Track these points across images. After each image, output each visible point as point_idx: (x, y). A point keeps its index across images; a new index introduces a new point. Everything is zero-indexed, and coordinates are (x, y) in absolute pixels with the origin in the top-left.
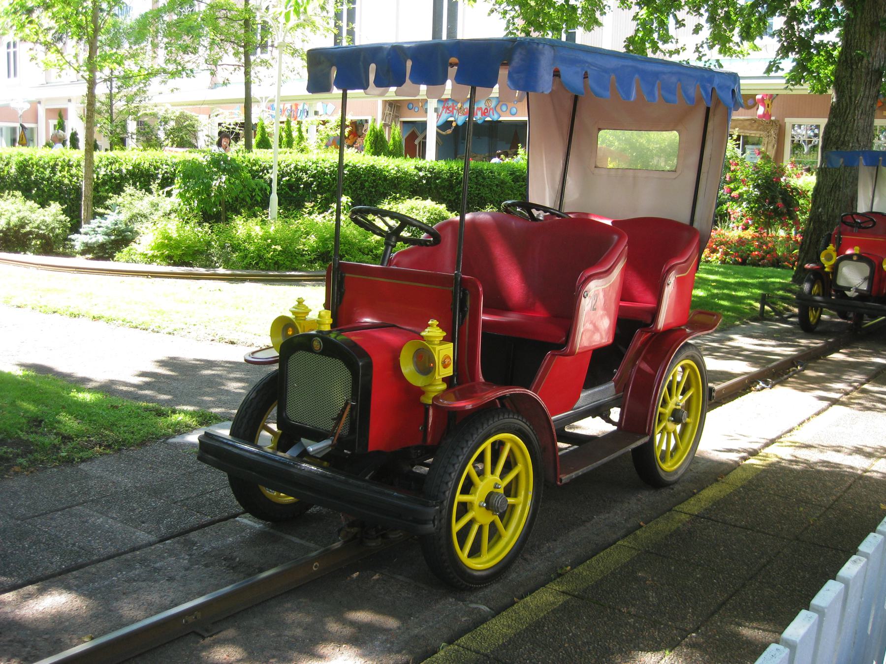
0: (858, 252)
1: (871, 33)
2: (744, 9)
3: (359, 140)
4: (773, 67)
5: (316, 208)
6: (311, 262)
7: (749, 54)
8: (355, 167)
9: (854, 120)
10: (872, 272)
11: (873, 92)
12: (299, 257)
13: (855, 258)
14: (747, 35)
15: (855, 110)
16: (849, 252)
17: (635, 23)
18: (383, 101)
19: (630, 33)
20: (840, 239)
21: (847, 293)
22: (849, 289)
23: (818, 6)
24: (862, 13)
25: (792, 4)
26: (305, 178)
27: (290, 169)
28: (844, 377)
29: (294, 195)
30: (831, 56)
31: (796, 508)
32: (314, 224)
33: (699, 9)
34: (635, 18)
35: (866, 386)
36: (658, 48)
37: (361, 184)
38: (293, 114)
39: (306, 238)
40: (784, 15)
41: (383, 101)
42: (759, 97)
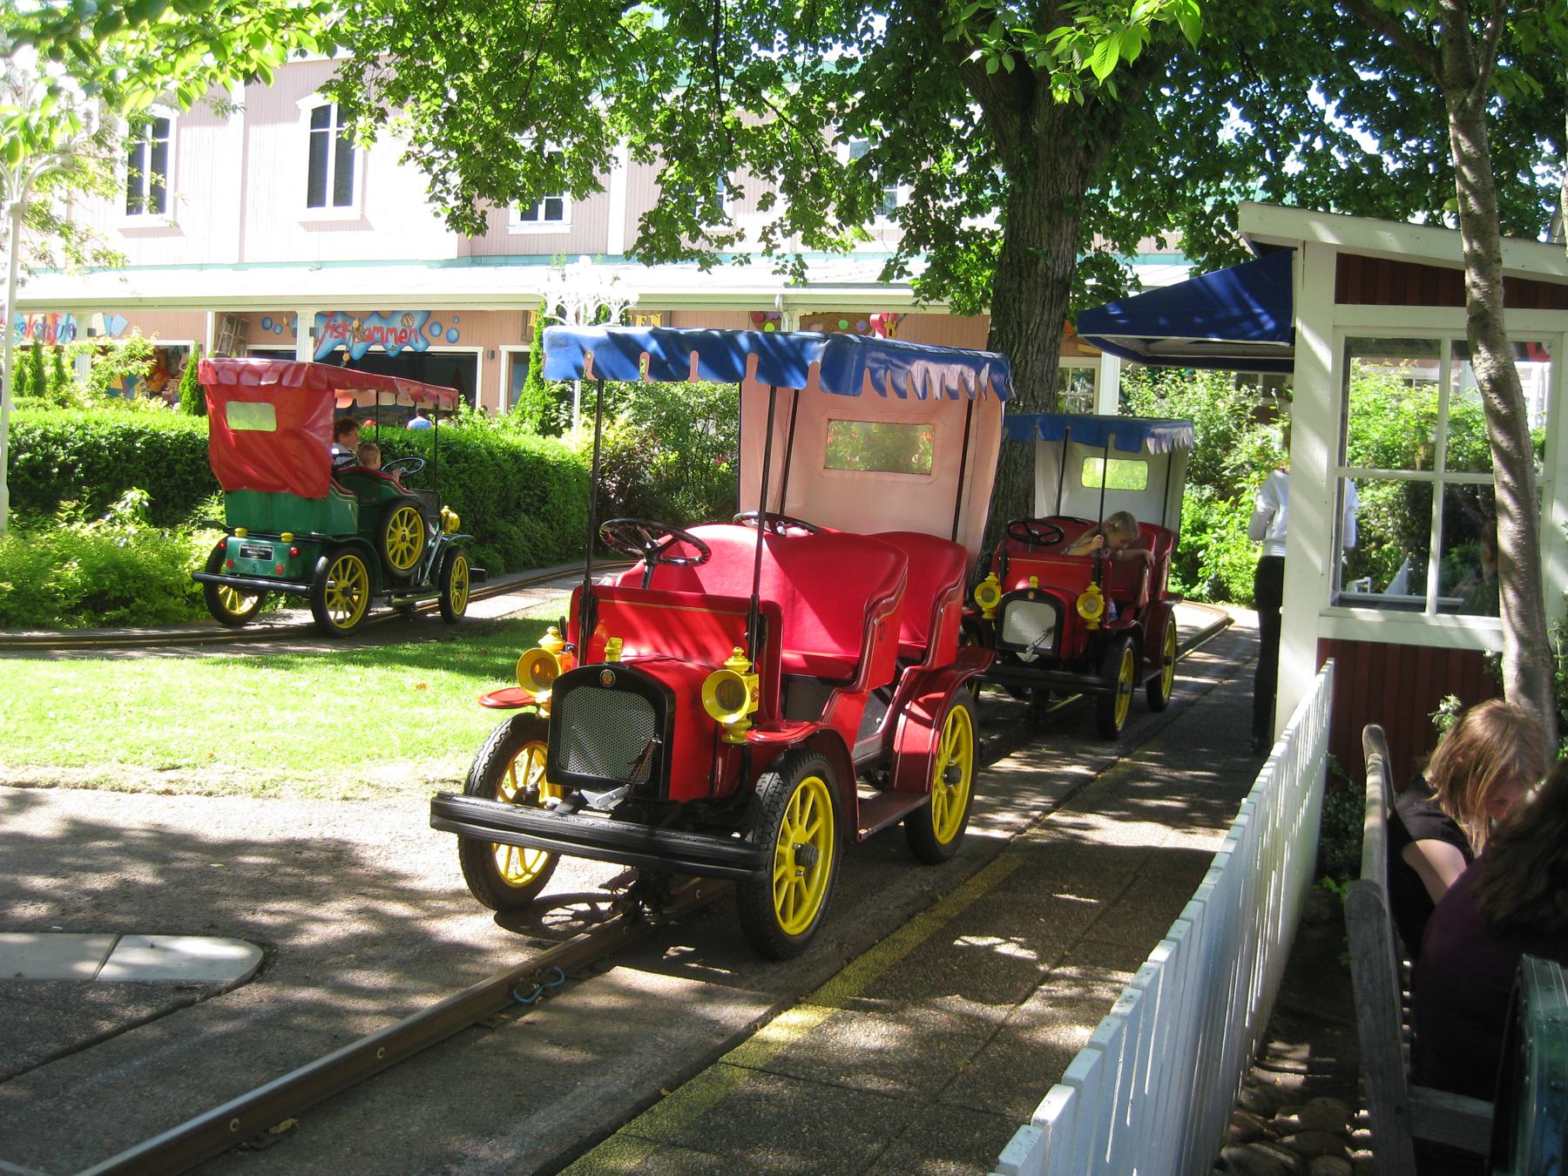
0: (1036, 586)
1: (1049, 218)
2: (845, 172)
3: (172, 382)
4: (893, 270)
5: (81, 512)
6: (74, 611)
7: (853, 246)
8: (156, 435)
9: (1027, 362)
10: (1059, 619)
11: (1056, 318)
12: (47, 604)
13: (1031, 596)
14: (850, 214)
15: (1027, 344)
16: (1020, 586)
17: (659, 187)
18: (217, 313)
19: (652, 205)
20: (1006, 563)
21: (1020, 655)
22: (1023, 648)
23: (965, 170)
24: (1035, 187)
25: (925, 165)
26: (62, 455)
27: (33, 440)
28: (1018, 801)
29: (41, 486)
30: (987, 253)
31: (934, 1044)
32: (74, 543)
33: (771, 168)
34: (659, 180)
35: (1053, 816)
36: (699, 232)
37: (168, 466)
38: (48, 332)
39: (60, 567)
40: (911, 182)
41: (217, 313)
42: (875, 317)
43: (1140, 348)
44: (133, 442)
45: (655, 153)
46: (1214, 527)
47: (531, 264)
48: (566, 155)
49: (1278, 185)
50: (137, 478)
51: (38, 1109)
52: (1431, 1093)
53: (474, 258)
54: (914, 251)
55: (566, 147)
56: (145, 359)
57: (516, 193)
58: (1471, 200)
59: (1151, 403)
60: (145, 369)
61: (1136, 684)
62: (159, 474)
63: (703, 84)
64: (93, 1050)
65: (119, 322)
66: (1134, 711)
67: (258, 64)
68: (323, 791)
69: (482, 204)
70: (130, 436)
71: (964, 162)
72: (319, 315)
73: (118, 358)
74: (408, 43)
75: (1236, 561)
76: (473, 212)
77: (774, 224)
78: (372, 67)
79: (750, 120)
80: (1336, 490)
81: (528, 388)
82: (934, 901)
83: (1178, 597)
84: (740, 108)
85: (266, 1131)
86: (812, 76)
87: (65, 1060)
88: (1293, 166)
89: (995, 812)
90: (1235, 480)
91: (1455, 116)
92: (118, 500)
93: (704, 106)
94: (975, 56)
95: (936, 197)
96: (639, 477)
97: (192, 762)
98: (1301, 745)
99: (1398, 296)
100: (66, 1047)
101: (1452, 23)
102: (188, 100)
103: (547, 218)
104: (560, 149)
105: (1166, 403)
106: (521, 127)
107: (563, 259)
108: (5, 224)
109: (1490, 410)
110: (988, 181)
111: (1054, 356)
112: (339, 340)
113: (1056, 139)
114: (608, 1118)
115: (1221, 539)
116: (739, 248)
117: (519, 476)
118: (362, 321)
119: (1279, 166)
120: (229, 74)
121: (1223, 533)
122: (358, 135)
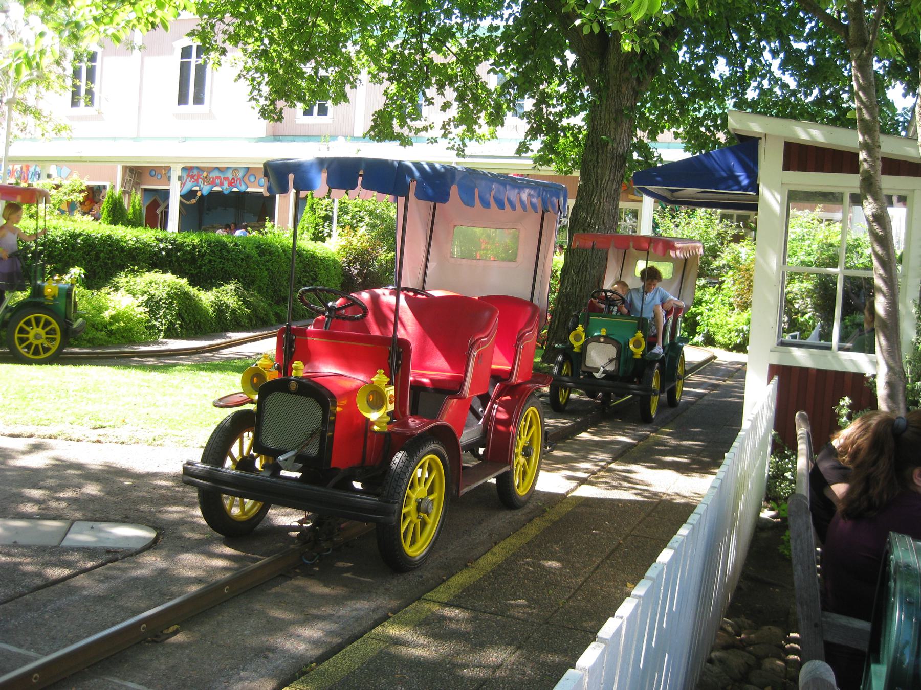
0: (605, 334)
3: (96, 207)
4: (523, 148)
8: (89, 236)
9: (600, 203)
11: (618, 177)
21: (595, 374)
22: (597, 370)
24: (607, 100)
25: (541, 87)
30: (576, 139)
31: (545, 591)
35: (613, 466)
40: (533, 97)
43: (667, 195)
44: (76, 240)
45: (383, 78)
46: (706, 302)
47: (309, 141)
48: (331, 78)
49: (741, 104)
50: (78, 261)
51: (29, 617)
52: (835, 616)
53: (276, 137)
54: (534, 138)
55: (331, 73)
56: (81, 191)
57: (301, 99)
58: (864, 111)
59: (669, 230)
60: (81, 197)
61: (662, 391)
62: (91, 259)
63: (412, 37)
64: (59, 585)
65: (66, 170)
66: (661, 406)
67: (161, 19)
68: (189, 443)
69: (281, 104)
70: (74, 236)
71: (565, 85)
72: (184, 169)
73: (65, 191)
74: (242, 10)
75: (719, 322)
76: (275, 109)
77: (450, 119)
78: (219, 22)
79: (438, 59)
80: (781, 278)
81: (306, 213)
82: (544, 511)
83: (686, 341)
84: (433, 52)
85: (162, 632)
86: (473, 36)
87: (44, 590)
88: (751, 94)
89: (578, 462)
90: (720, 275)
91: (856, 62)
92: (67, 273)
93: (413, 51)
94: (578, 22)
95: (548, 106)
96: (370, 266)
97: (112, 424)
98: (759, 425)
99: (819, 168)
100: (44, 583)
101: (855, 9)
102: (118, 40)
103: (318, 114)
104: (327, 74)
105: (679, 230)
106: (306, 59)
107: (328, 138)
108: (5, 108)
109: (872, 233)
110: (578, 97)
111: (616, 200)
112: (196, 183)
113: (620, 73)
114: (358, 629)
115: (711, 310)
116: (431, 134)
117: (301, 265)
118: (209, 173)
119: (744, 93)
120: (143, 24)
121: (712, 306)
122: (211, 62)
